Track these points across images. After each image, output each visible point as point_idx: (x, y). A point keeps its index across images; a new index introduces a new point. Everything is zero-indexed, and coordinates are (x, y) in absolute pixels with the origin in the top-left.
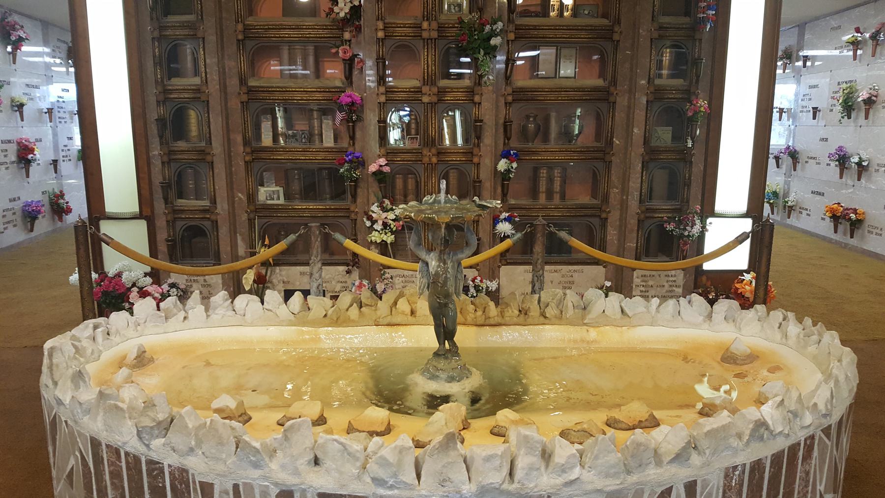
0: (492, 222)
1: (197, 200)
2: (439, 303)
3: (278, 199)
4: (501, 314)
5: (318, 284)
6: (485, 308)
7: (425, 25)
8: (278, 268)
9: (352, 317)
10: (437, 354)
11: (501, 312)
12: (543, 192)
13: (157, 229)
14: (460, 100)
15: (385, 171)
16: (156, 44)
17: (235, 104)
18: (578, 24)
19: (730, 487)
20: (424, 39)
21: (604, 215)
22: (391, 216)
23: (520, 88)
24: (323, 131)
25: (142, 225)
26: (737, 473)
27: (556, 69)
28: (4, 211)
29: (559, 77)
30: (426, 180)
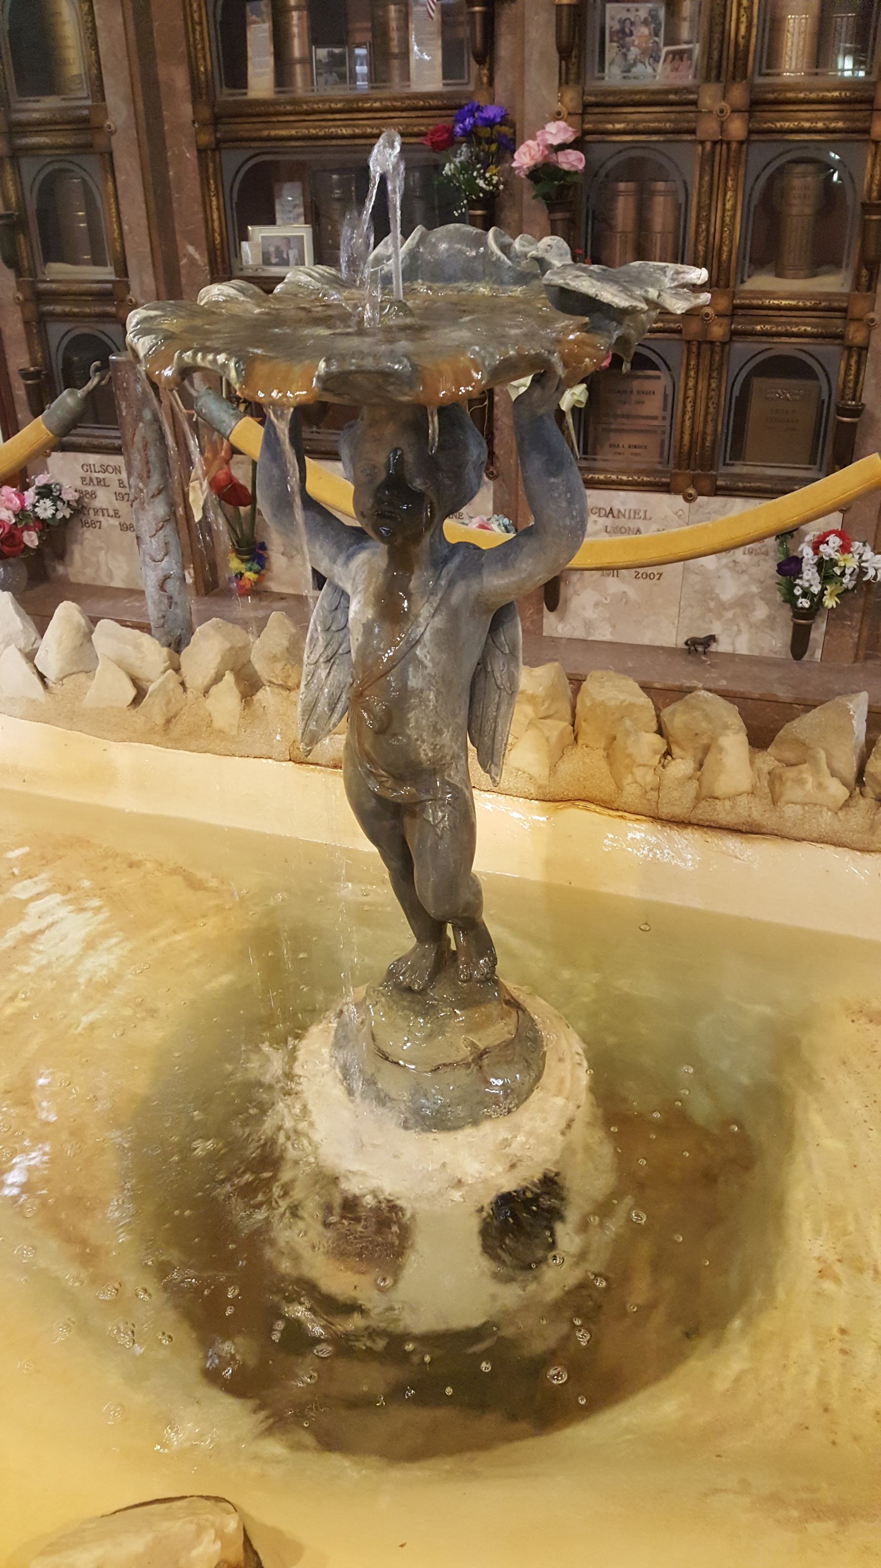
2: (377, 796)
4: (771, 784)
5: (160, 574)
6: (706, 749)
9: (220, 722)
11: (774, 778)
15: (565, 167)
30: (705, 200)
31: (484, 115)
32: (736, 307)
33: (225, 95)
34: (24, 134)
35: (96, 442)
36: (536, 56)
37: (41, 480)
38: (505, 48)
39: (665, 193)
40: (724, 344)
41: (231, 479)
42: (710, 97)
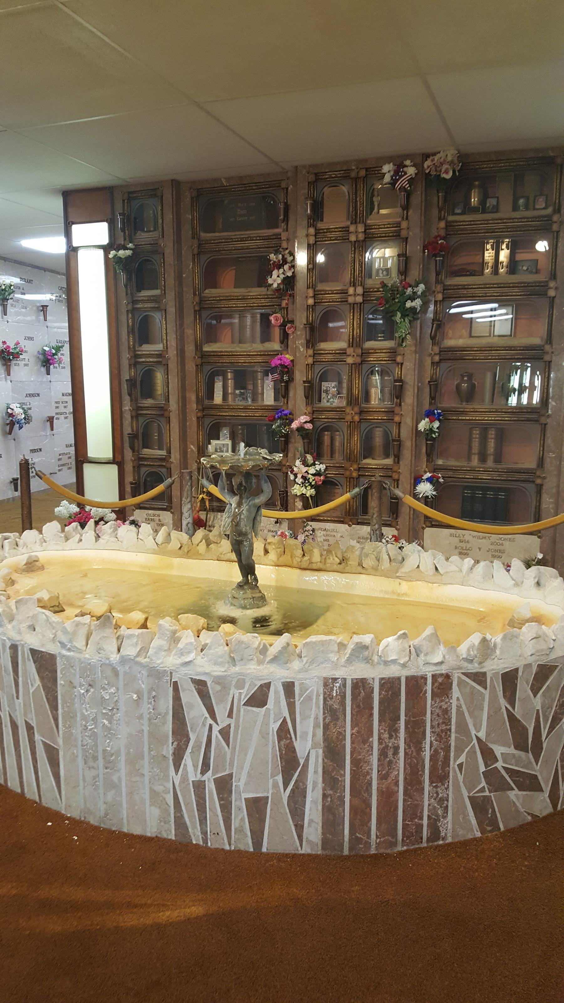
0: (412, 481)
1: (159, 450)
2: (235, 540)
3: (227, 451)
5: (187, 522)
7: (351, 291)
8: (219, 513)
10: (240, 586)
12: (475, 454)
13: (125, 473)
14: (382, 361)
16: (130, 315)
17: (191, 366)
18: (510, 282)
19: (331, 696)
20: (350, 304)
21: (539, 481)
22: (312, 470)
23: (448, 348)
24: (265, 391)
25: (114, 469)
26: (338, 685)
27: (515, 328)
28: (60, 455)
29: (494, 336)
31: (284, 413)
32: (359, 468)
33: (206, 402)
34: (142, 410)
35: (152, 506)
36: (299, 397)
37: (132, 518)
38: (291, 394)
39: (327, 435)
40: (357, 478)
41: (199, 517)
42: (348, 410)
